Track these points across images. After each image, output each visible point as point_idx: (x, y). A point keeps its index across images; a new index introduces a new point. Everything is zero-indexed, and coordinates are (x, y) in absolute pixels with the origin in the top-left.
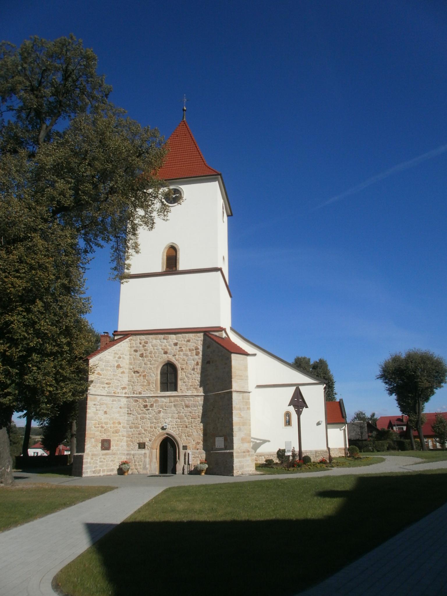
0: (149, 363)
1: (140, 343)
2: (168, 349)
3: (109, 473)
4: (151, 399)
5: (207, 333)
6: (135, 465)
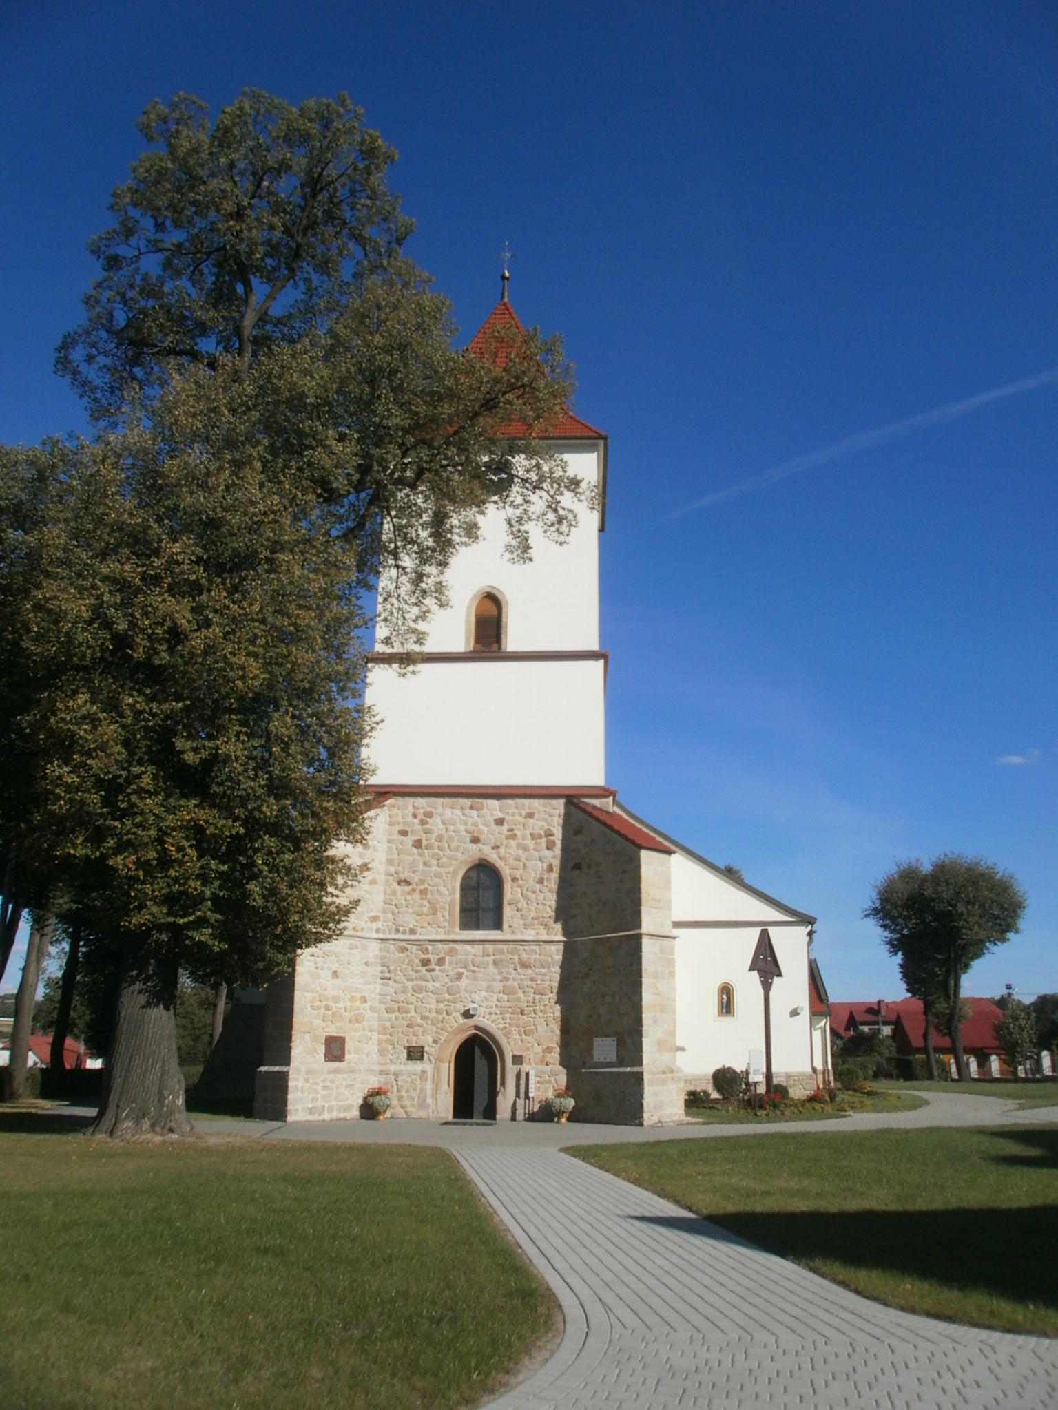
0: (435, 862)
1: (415, 816)
2: (481, 831)
3: (342, 1115)
4: (440, 946)
5: (575, 800)
6: (400, 1098)
